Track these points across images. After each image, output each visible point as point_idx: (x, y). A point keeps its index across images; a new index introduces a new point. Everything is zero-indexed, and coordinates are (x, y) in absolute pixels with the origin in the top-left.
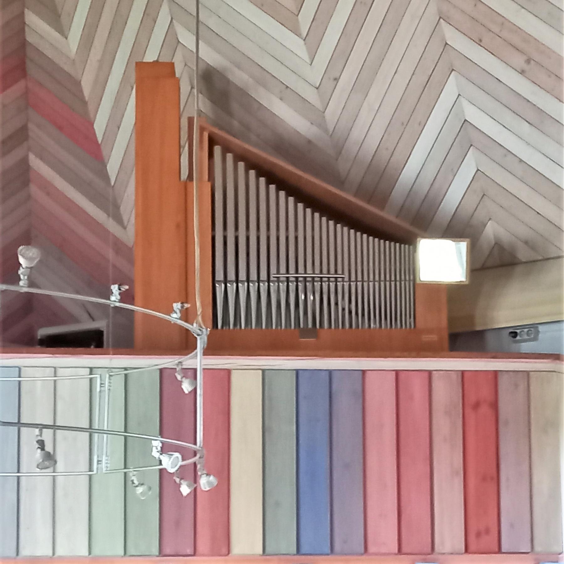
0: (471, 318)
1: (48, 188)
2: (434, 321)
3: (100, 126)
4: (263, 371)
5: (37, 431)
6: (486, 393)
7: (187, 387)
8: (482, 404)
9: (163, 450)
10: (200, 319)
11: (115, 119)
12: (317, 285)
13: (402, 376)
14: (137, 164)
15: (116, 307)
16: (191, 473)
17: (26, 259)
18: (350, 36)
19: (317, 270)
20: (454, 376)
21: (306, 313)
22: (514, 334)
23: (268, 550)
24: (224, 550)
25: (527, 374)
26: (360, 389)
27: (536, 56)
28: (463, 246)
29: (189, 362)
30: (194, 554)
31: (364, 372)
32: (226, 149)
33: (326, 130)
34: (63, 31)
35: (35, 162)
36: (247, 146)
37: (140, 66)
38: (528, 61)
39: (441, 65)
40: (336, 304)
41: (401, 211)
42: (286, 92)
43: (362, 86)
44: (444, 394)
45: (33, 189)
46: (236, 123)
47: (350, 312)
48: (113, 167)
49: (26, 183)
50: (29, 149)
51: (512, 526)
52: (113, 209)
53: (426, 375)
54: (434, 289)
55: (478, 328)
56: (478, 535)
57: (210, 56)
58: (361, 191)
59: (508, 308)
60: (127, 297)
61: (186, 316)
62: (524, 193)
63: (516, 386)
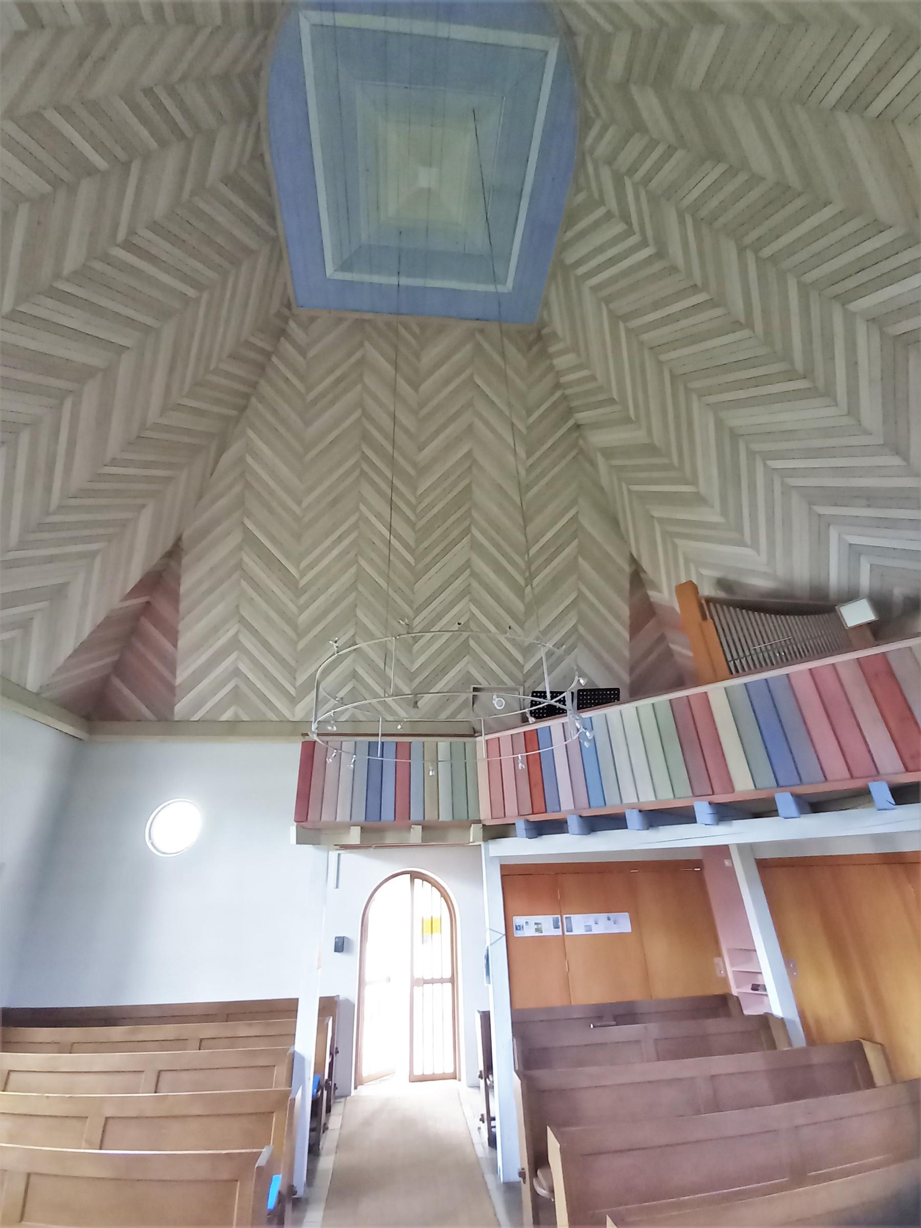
13: (791, 676)
34: (660, 591)
38: (868, 499)
57: (717, 574)
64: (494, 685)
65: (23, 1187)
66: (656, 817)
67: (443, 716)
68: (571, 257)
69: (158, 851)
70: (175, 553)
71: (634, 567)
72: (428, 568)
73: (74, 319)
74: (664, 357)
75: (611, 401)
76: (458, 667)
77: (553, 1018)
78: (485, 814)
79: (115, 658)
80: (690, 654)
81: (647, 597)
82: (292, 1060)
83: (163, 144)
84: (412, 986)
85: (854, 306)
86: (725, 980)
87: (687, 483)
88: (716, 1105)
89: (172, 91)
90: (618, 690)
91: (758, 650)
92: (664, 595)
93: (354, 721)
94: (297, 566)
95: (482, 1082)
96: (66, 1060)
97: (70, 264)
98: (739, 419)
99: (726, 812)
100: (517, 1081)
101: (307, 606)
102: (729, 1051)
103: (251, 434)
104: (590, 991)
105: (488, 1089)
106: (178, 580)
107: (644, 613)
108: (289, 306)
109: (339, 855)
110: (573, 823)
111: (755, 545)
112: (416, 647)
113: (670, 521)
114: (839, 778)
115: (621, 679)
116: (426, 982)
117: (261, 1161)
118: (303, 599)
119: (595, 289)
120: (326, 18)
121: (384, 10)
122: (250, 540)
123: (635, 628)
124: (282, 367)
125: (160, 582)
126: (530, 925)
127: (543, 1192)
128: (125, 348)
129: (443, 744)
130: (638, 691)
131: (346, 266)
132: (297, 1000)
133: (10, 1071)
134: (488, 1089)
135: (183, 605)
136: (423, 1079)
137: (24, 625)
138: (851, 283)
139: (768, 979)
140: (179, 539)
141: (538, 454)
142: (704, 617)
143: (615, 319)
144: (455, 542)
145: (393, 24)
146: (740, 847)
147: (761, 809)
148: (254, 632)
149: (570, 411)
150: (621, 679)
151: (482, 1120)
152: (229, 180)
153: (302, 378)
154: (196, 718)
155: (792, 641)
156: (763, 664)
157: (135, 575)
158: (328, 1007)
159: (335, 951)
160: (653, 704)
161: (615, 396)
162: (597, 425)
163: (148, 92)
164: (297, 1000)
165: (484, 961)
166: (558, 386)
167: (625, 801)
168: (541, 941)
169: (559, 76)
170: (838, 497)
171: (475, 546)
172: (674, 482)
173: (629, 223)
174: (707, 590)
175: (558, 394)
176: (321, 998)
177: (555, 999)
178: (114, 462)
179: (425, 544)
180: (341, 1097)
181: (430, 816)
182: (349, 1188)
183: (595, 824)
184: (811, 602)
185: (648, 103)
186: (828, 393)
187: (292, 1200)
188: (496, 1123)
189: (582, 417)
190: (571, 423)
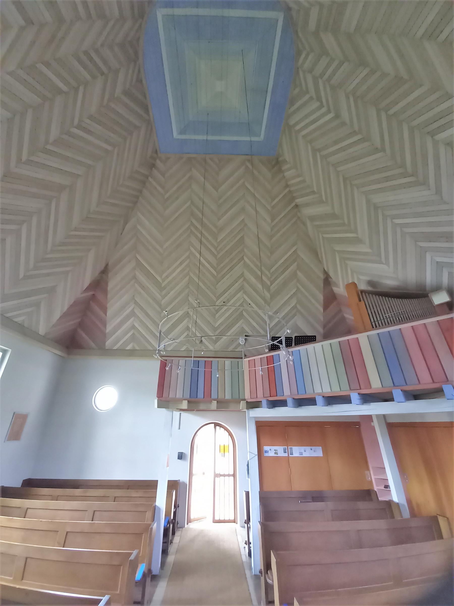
44: (434, 331)
57: (368, 278)
64: (255, 334)
65: (24, 563)
66: (331, 400)
67: (231, 349)
68: (292, 122)
69: (98, 409)
70: (105, 271)
71: (325, 276)
72: (223, 277)
73: (54, 163)
74: (339, 169)
75: (313, 192)
76: (238, 325)
77: (283, 496)
78: (247, 396)
79: (79, 320)
80: (352, 318)
81: (332, 290)
82: (155, 509)
83: (94, 77)
84: (214, 477)
85: (437, 137)
86: (371, 482)
87: (351, 232)
88: (360, 546)
89: (97, 51)
90: (315, 336)
91: (388, 317)
92: (340, 290)
93: (187, 350)
94: (161, 276)
95: (246, 525)
96: (52, 504)
97: (52, 137)
98: (377, 199)
99: (367, 398)
100: (259, 526)
101: (166, 295)
102: (370, 518)
103: (139, 215)
104: (301, 484)
105: (248, 529)
106: (107, 284)
107: (330, 299)
108: (156, 152)
109: (180, 414)
110: (290, 402)
111: (387, 263)
112: (217, 316)
113: (343, 252)
114: (426, 383)
115: (318, 331)
116: (221, 475)
117: (132, 557)
118: (164, 292)
119: (304, 137)
120: (169, 11)
121: (197, 5)
122: (139, 264)
123: (326, 306)
124: (154, 183)
125: (99, 285)
126: (271, 451)
127: (269, 581)
128: (79, 175)
129: (228, 362)
130: (327, 336)
131: (182, 132)
132: (157, 481)
133: (28, 508)
134: (248, 529)
135: (109, 296)
136: (220, 521)
137: (37, 305)
138: (435, 125)
139: (391, 483)
140: (107, 265)
141: (277, 220)
142: (360, 301)
143: (314, 151)
144: (235, 265)
145: (201, 12)
146: (378, 416)
147: (387, 398)
148: (142, 309)
149: (293, 199)
150: (318, 331)
151: (246, 543)
152: (126, 93)
153: (163, 187)
154: (115, 348)
155: (406, 312)
156: (384, 325)
157: (87, 283)
158: (173, 485)
159: (178, 459)
160: (330, 344)
161: (315, 190)
162: (307, 205)
163: (86, 53)
164: (157, 481)
165: (246, 467)
166: (287, 186)
167: (315, 392)
168: (277, 459)
169: (284, 30)
170: (430, 237)
171: (246, 266)
172: (346, 232)
173: (321, 102)
174: (362, 286)
175: (287, 190)
176: (168, 481)
177: (283, 487)
178: (76, 229)
179: (222, 265)
180: (181, 528)
181: (221, 396)
182: (181, 571)
183: (301, 402)
184: (391, 291)
185: (329, 40)
186: (425, 183)
187: (151, 577)
188: (251, 545)
189: (299, 201)
190: (293, 204)
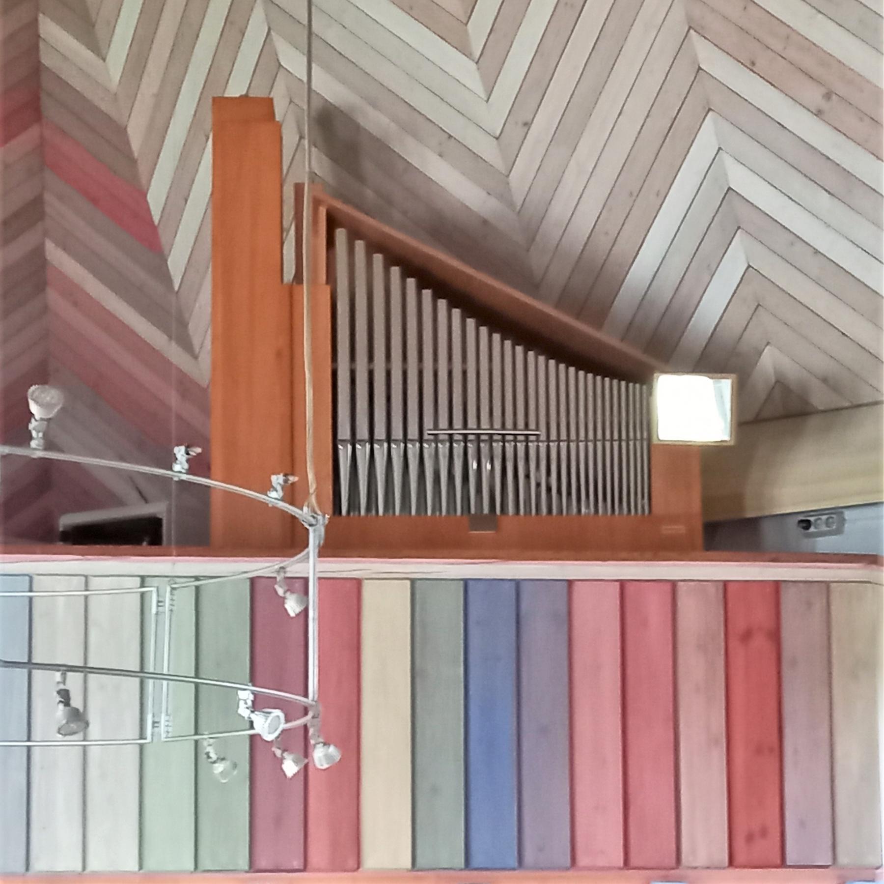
0: (738, 499)
1: (75, 295)
2: (680, 503)
3: (156, 198)
4: (413, 581)
5: (58, 676)
6: (761, 615)
7: (292, 607)
8: (756, 634)
9: (256, 706)
10: (313, 499)
11: (180, 186)
12: (497, 446)
13: (630, 589)
14: (214, 256)
15: (182, 482)
16: (300, 741)
17: (41, 405)
18: (548, 56)
19: (497, 424)
20: (712, 589)
21: (479, 490)
22: (806, 524)
23: (420, 862)
24: (352, 863)
25: (826, 586)
26: (564, 610)
27: (840, 89)
28: (726, 385)
29: (296, 567)
30: (305, 869)
31: (570, 583)
32: (354, 234)
33: (511, 204)
34: (98, 49)
35: (55, 254)
36: (387, 229)
37: (220, 103)
38: (828, 96)
39: (691, 101)
40: (527, 476)
41: (629, 331)
42: (448, 144)
43: (568, 134)
44: (697, 618)
45: (52, 296)
46: (369, 193)
47: (549, 489)
48: (177, 262)
49: (41, 287)
50: (46, 234)
51: (802, 824)
52: (177, 328)
53: (668, 587)
54: (680, 453)
55: (750, 514)
56: (750, 838)
57: (329, 88)
58: (565, 299)
59: (796, 483)
60: (198, 465)
61: (292, 495)
62: (821, 302)
63: (809, 604)
